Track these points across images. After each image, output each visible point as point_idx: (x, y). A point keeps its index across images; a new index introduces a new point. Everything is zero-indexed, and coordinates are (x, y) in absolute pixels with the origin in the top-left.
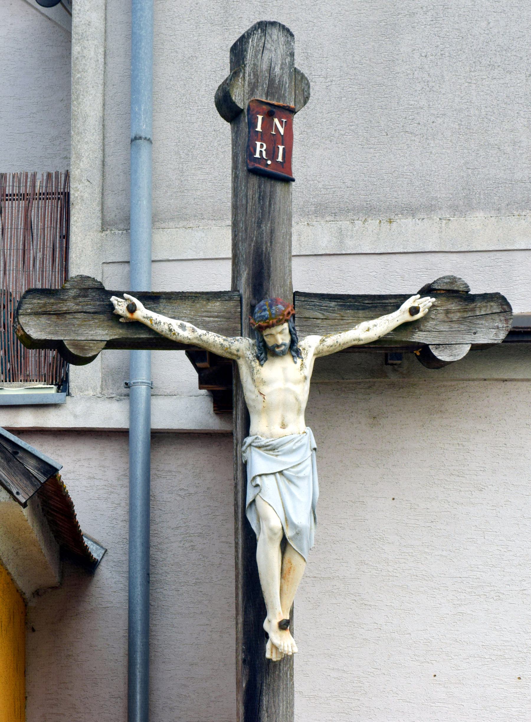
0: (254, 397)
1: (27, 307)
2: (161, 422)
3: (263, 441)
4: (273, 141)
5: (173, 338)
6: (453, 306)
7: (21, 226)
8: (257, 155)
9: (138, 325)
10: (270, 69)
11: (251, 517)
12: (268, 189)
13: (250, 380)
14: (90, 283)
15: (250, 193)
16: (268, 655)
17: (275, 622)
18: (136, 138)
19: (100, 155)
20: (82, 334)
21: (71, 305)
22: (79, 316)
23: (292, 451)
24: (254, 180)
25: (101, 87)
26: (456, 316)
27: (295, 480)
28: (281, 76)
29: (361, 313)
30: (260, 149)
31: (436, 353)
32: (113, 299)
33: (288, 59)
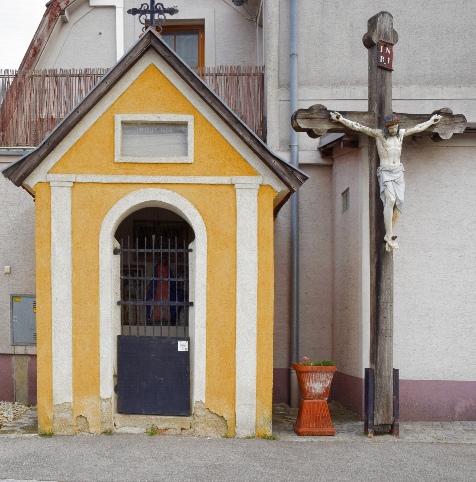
0: (383, 151)
1: (300, 115)
2: (302, 161)
3: (387, 168)
4: (387, 56)
5: (353, 129)
6: (447, 119)
7: (246, 86)
8: (381, 61)
9: (339, 123)
10: (385, 29)
11: (382, 198)
12: (384, 74)
13: (381, 145)
14: (322, 107)
15: (378, 75)
16: (387, 250)
17: (390, 237)
18: (293, 54)
19: (277, 60)
20: (319, 127)
21: (315, 115)
22: (318, 119)
23: (397, 172)
24: (380, 70)
25: (278, 35)
26: (448, 123)
27: (399, 183)
28: (389, 32)
29: (416, 121)
30: (382, 58)
31: (441, 136)
32: (331, 113)
33: (391, 26)
